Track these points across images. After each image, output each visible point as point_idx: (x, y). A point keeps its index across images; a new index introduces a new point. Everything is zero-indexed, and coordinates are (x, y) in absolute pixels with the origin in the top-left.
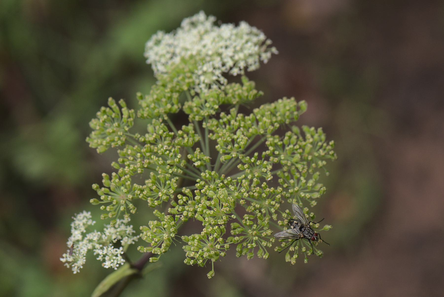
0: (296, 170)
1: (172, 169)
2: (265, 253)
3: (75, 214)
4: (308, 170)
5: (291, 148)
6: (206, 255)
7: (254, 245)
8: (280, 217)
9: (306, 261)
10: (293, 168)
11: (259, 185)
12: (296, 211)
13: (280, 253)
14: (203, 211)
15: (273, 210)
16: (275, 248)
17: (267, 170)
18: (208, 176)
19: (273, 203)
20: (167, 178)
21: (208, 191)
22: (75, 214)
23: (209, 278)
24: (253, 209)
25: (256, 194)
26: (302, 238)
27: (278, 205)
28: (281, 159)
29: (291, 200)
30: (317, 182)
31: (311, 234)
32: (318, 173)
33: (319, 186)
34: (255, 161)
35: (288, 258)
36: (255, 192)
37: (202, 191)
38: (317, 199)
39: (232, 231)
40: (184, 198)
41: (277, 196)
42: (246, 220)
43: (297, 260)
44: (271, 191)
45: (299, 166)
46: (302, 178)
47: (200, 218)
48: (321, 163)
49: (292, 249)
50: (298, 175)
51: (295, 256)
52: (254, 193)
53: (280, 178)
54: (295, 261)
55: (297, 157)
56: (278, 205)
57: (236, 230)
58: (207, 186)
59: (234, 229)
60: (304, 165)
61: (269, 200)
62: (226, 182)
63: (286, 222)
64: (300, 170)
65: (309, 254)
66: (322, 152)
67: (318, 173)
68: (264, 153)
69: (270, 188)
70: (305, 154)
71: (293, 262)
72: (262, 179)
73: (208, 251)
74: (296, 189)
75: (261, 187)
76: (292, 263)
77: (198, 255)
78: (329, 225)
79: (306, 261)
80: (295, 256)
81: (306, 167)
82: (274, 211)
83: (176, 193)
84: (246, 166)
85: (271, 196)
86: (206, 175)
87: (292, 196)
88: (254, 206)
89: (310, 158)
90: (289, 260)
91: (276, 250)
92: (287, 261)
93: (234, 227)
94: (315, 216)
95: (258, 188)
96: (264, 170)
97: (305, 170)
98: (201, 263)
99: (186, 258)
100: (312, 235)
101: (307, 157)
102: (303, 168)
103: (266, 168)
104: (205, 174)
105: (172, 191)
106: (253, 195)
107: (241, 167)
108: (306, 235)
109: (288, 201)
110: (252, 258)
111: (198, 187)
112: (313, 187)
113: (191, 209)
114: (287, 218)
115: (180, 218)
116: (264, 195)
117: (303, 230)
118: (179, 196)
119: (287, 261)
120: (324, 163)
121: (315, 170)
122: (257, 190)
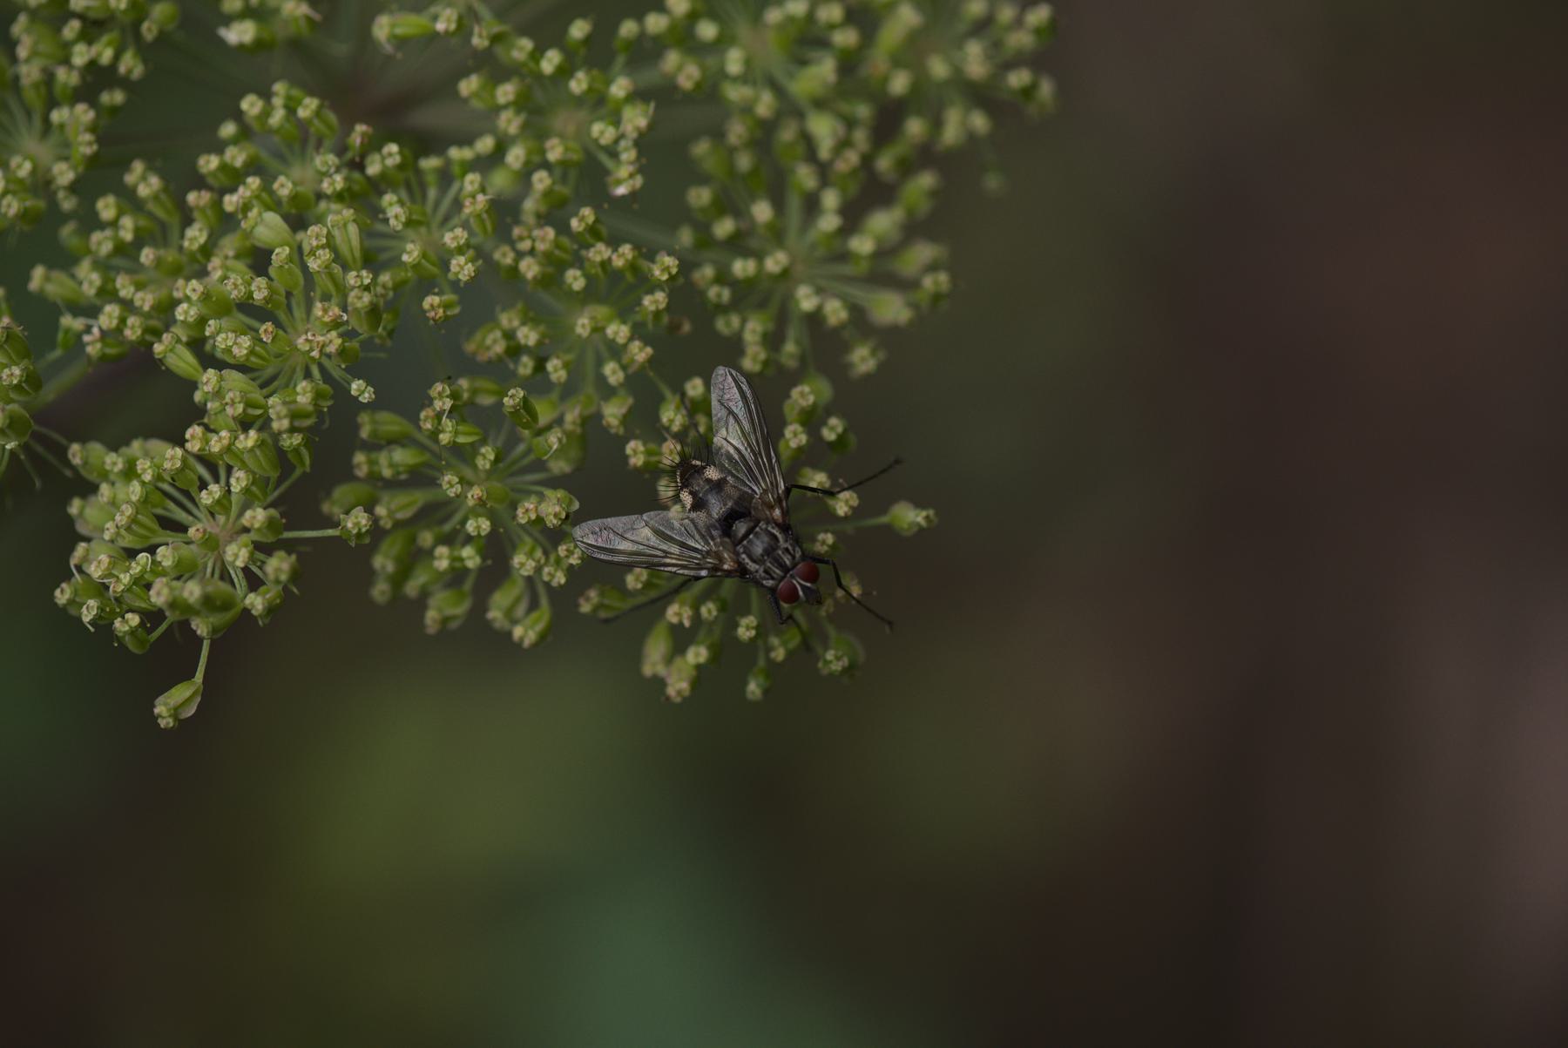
0: (800, 150)
1: (90, 43)
2: (534, 605)
3: (89, 79)
4: (867, 161)
5: (791, 19)
6: (159, 595)
7: (470, 557)
8: (644, 420)
9: (754, 688)
10: (787, 134)
11: (555, 214)
12: (730, 412)
13: (607, 621)
14: (202, 322)
15: (613, 373)
16: (581, 593)
17: (622, 136)
18: (277, 117)
19: (618, 331)
20: (58, 90)
21: (253, 214)
22: (89, 79)
23: (162, 723)
24: (499, 348)
25: (530, 269)
26: (729, 573)
27: (640, 353)
28: (723, 75)
29: (735, 321)
30: (913, 230)
31: (782, 566)
32: (926, 180)
33: (923, 252)
34: (565, 72)
35: (654, 657)
36: (532, 252)
37: (231, 202)
38: (888, 337)
39: (360, 458)
40: (127, 222)
41: (647, 301)
42: (439, 416)
43: (701, 675)
44: (618, 263)
45: (823, 128)
46: (831, 199)
47: (182, 361)
48: (961, 124)
49: (677, 613)
50: (805, 176)
51: (697, 655)
52: (520, 255)
53: (703, 179)
54: (684, 686)
55: (824, 70)
56: (640, 353)
57: (383, 458)
58: (254, 182)
59: (373, 446)
60: (850, 123)
61: (602, 311)
62: (373, 169)
63: (670, 453)
64: (824, 153)
65: (779, 654)
66: (975, 60)
67: (926, 180)
68: (628, 28)
69: (614, 243)
70: (878, 60)
71: (678, 686)
72: (588, 174)
73: (183, 572)
74: (775, 262)
75: (563, 228)
76: (671, 692)
77: (126, 579)
78: (919, 504)
79: (754, 688)
80: (697, 655)
81: (861, 137)
82: (620, 376)
83: (87, 189)
84: (506, 92)
85: (618, 289)
86: (266, 113)
87: (747, 295)
88: (509, 335)
89: (899, 84)
90: (661, 670)
91: (585, 608)
92: (647, 670)
93: (374, 433)
94: (852, 439)
95: (550, 233)
96: (602, 131)
97: (852, 158)
98: (133, 632)
99: (68, 576)
100: (786, 570)
101: (885, 80)
102: (843, 144)
103: (617, 122)
104: (276, 106)
105: (64, 174)
106: (514, 270)
107: (476, 95)
108: (752, 566)
109: (721, 325)
110: (454, 625)
111: (213, 174)
112: (884, 253)
113: (145, 300)
114: (680, 437)
115: (79, 336)
116: (575, 280)
117: (741, 528)
118: (106, 207)
119: (647, 670)
120: (980, 122)
121: (926, 155)
122: (541, 247)
